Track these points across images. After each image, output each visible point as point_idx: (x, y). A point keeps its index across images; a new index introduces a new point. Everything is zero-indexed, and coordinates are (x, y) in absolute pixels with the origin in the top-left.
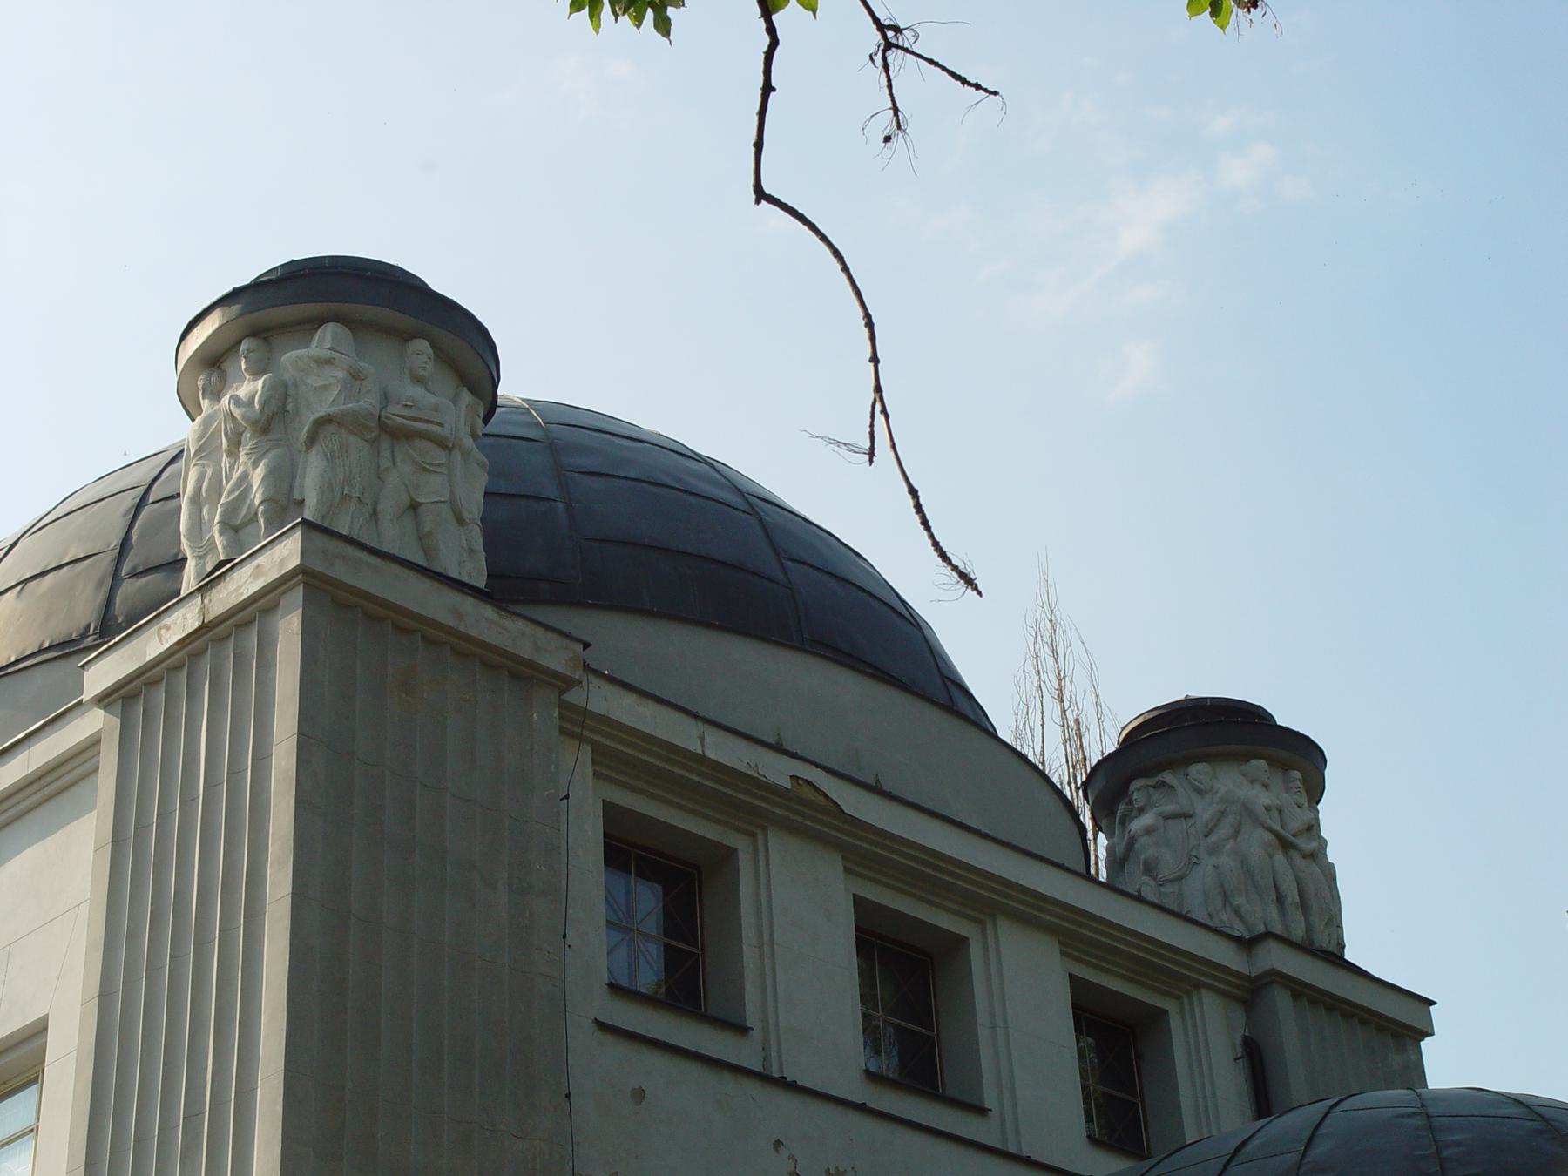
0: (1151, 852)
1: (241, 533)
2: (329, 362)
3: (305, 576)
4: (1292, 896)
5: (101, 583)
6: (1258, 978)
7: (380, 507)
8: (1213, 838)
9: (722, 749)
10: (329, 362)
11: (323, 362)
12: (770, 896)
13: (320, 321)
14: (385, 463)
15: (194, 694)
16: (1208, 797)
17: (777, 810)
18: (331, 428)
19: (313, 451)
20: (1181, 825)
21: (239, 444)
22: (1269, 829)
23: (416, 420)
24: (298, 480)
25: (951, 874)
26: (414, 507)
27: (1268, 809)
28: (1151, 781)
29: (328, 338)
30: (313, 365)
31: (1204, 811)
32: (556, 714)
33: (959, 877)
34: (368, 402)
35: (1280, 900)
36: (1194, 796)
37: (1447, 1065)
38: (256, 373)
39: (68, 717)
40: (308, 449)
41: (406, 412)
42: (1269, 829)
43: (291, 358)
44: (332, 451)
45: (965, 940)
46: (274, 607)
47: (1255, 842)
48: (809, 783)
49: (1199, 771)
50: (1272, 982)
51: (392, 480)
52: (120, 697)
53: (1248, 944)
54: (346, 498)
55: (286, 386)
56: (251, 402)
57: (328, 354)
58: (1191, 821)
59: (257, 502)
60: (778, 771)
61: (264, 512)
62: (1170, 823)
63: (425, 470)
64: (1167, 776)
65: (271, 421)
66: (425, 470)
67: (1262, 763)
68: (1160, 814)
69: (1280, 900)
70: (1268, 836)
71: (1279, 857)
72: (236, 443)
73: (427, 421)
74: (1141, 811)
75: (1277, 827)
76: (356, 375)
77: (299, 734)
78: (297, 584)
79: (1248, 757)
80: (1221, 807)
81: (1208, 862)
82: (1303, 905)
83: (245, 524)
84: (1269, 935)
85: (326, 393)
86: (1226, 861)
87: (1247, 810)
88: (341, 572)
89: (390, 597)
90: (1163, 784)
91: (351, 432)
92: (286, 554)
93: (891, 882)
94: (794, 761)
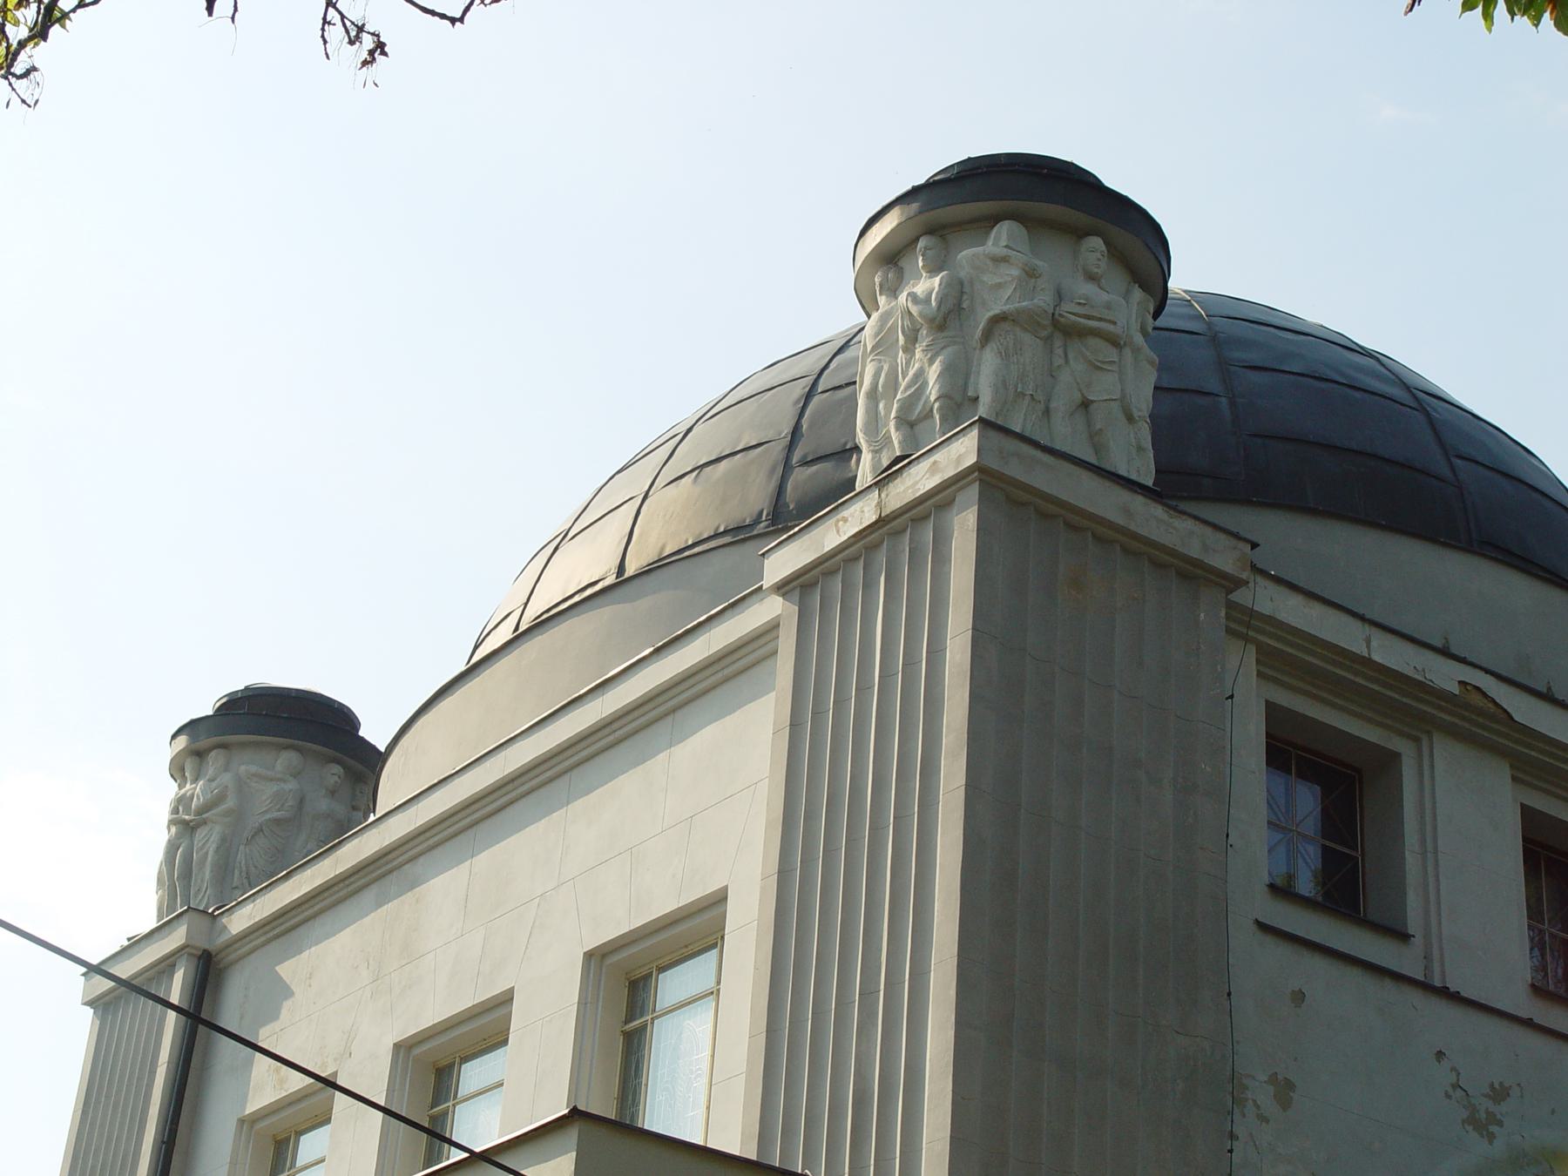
1: (918, 428)
2: (1005, 260)
3: (980, 472)
7: (1053, 405)
9: (1388, 653)
10: (1005, 260)
13: (995, 220)
15: (870, 586)
18: (1006, 326)
19: (988, 350)
21: (916, 340)
26: (1085, 404)
29: (1004, 236)
30: (989, 262)
34: (1043, 300)
38: (933, 270)
39: (747, 601)
43: (966, 255)
51: (1065, 377)
56: (928, 300)
57: (1005, 252)
59: (932, 398)
60: (1446, 675)
61: (940, 409)
65: (948, 318)
72: (912, 339)
73: (1100, 319)
76: (1031, 273)
85: (1000, 291)
88: (1015, 471)
89: (1064, 496)
91: (1026, 330)
92: (963, 451)
94: (1462, 666)
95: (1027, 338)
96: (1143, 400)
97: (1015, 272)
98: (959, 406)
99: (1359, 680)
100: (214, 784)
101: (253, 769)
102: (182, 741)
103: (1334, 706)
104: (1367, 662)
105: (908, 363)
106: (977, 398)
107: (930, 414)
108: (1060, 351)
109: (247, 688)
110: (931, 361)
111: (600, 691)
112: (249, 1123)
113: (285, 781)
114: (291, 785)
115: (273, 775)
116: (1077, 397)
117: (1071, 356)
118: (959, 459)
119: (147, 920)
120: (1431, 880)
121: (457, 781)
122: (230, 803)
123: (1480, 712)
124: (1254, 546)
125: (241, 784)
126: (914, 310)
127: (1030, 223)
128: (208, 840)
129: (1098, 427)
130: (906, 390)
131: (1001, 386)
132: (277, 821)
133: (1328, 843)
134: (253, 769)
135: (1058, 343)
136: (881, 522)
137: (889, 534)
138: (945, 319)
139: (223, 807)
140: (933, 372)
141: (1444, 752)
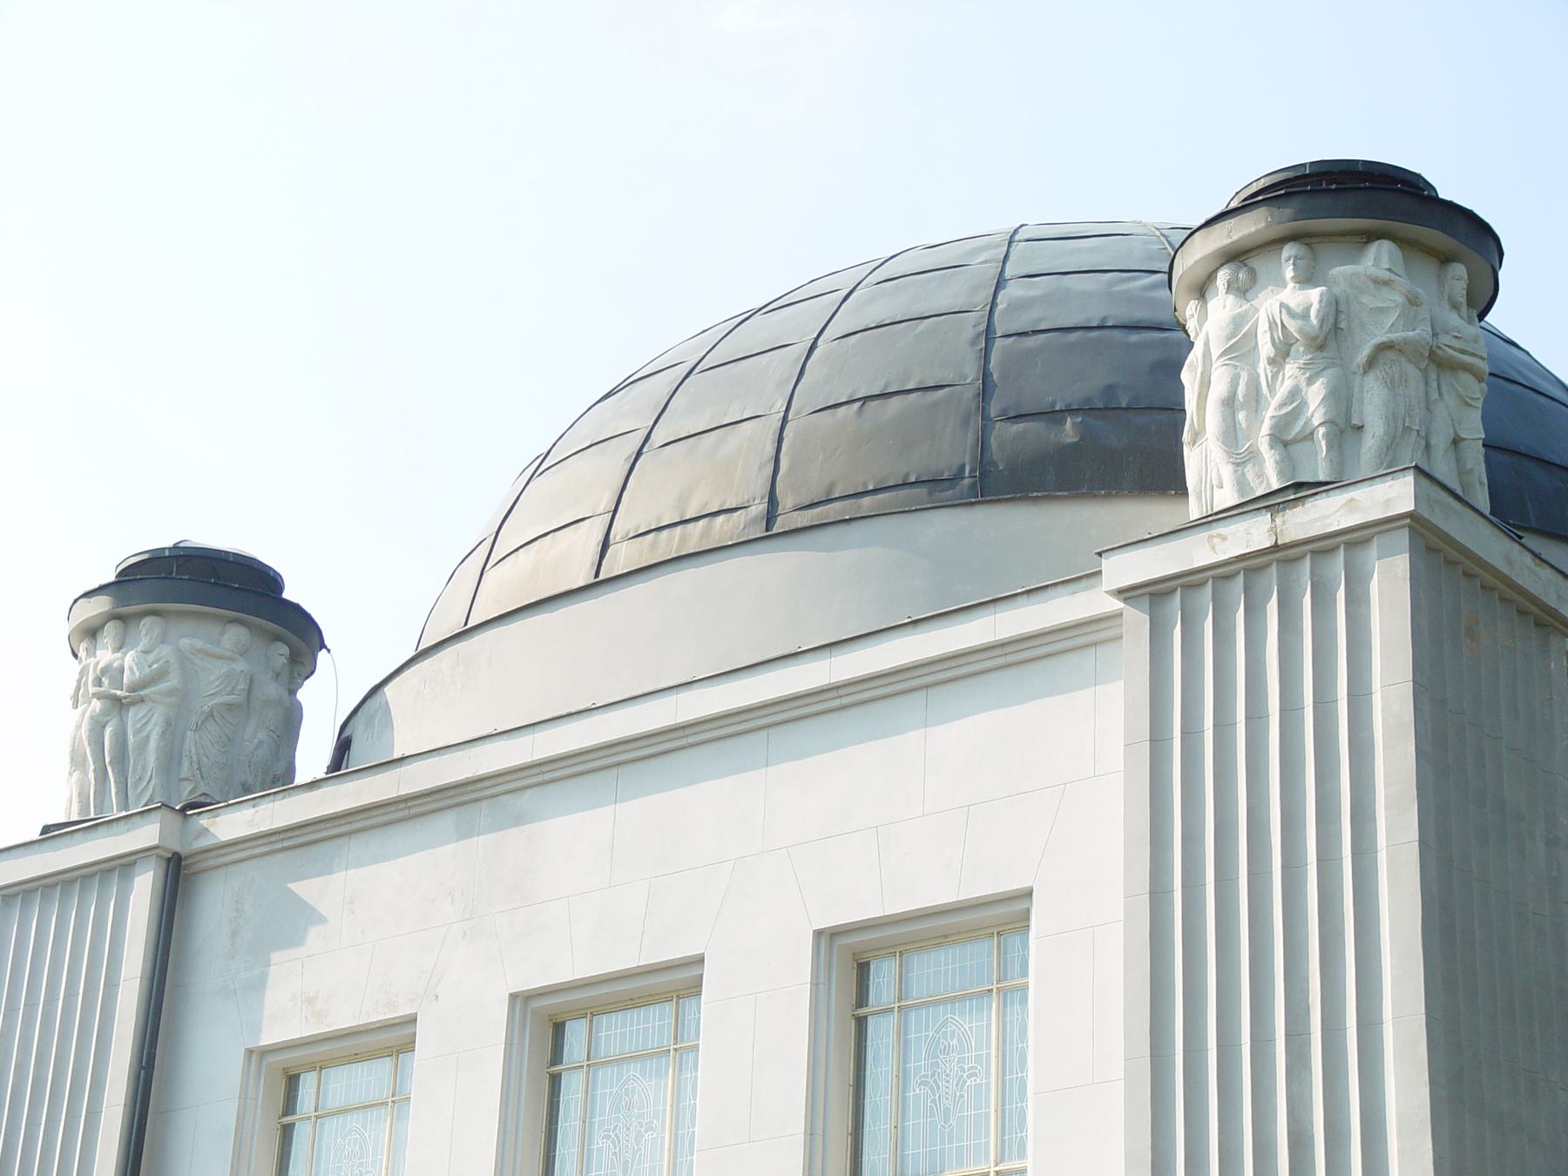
1: (1294, 449)
3: (1415, 523)
5: (966, 422)
13: (1370, 237)
14: (1435, 395)
18: (1390, 355)
19: (1371, 375)
23: (1462, 352)
24: (1355, 403)
29: (1385, 257)
34: (1421, 332)
37: (286, 595)
38: (1307, 279)
39: (1051, 592)
40: (1365, 372)
43: (1341, 271)
44: (1392, 380)
46: (1366, 541)
51: (1441, 412)
52: (1152, 594)
54: (1407, 429)
56: (1305, 315)
57: (1387, 275)
59: (1316, 422)
61: (1326, 435)
63: (1467, 404)
65: (1328, 339)
66: (1467, 404)
72: (1283, 352)
73: (1473, 355)
76: (1413, 301)
83: (1295, 441)
85: (1383, 319)
88: (1437, 519)
91: (1410, 361)
92: (1397, 495)
96: (1474, 431)
97: (1400, 299)
98: (1342, 432)
100: (151, 657)
101: (199, 644)
102: (102, 605)
105: (1275, 376)
106: (1360, 428)
107: (1310, 436)
108: (1434, 384)
109: (175, 547)
110: (1310, 381)
111: (826, 652)
112: (258, 1055)
113: (233, 660)
114: (241, 665)
115: (216, 650)
118: (1388, 503)
119: (59, 800)
121: (596, 718)
122: (173, 681)
125: (183, 659)
126: (1293, 326)
128: (147, 725)
130: (1282, 405)
132: (230, 707)
134: (199, 644)
136: (1276, 548)
139: (163, 686)
140: (1315, 395)
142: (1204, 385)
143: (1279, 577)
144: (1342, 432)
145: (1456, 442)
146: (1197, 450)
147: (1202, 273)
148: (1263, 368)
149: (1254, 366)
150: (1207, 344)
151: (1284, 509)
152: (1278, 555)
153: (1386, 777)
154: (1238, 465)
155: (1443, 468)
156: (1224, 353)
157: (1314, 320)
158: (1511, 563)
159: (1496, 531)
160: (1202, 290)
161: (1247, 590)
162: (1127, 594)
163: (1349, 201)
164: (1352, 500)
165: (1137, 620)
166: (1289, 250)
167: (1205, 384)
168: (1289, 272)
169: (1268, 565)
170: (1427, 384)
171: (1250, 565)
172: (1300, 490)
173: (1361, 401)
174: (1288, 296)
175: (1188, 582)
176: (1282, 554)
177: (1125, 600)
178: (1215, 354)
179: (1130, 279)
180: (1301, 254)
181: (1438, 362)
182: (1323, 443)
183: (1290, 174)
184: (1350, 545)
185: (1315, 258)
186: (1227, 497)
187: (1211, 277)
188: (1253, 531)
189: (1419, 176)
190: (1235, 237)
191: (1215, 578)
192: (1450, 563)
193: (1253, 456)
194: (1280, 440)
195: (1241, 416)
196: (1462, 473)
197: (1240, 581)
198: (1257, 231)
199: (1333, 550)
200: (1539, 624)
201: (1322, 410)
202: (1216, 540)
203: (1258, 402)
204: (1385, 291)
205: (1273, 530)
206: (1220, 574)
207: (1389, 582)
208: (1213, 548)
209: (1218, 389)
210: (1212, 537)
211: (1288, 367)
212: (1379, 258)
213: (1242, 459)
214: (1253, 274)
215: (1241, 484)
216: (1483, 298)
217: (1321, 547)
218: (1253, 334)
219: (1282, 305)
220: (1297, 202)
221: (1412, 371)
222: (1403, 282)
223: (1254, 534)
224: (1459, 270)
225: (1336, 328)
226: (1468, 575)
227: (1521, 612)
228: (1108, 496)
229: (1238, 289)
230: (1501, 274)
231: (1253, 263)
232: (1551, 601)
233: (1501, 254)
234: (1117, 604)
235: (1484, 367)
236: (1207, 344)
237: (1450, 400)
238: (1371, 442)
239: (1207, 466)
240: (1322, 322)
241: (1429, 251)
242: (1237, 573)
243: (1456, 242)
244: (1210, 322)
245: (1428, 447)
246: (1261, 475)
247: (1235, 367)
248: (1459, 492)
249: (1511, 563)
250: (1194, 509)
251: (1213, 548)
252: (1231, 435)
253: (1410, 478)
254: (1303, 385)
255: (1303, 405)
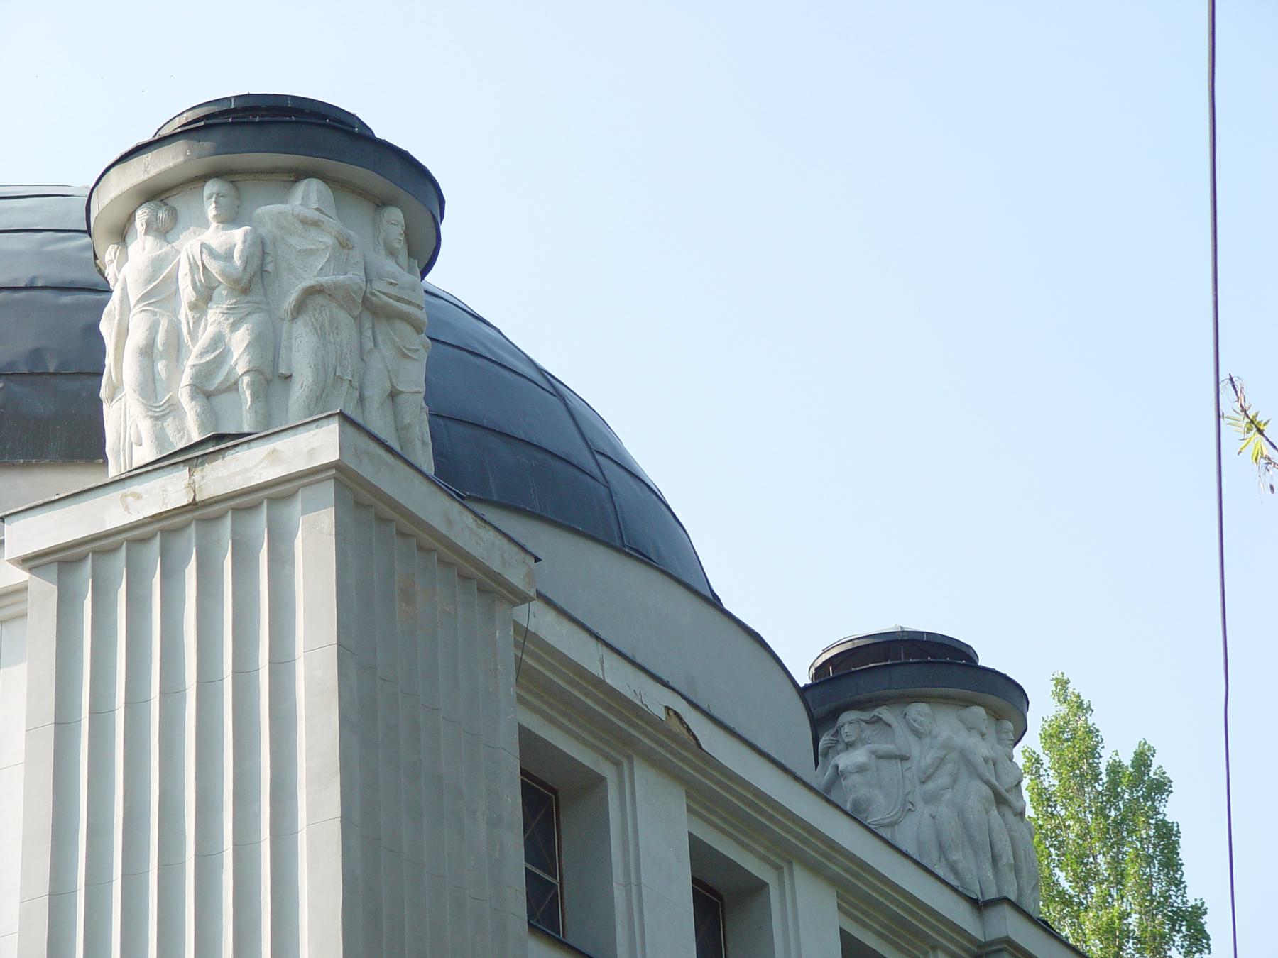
0: (862, 792)
1: (216, 400)
2: (315, 224)
3: (339, 473)
4: (1007, 858)
6: (988, 944)
7: (367, 393)
8: (930, 786)
9: (619, 677)
10: (315, 224)
11: (308, 223)
12: (636, 831)
13: (299, 175)
14: (369, 345)
15: (171, 577)
16: (928, 741)
17: (646, 741)
18: (320, 300)
20: (895, 767)
21: (209, 299)
22: (987, 783)
23: (399, 299)
24: (283, 353)
25: (770, 818)
26: (393, 395)
27: (986, 760)
28: (866, 716)
30: (300, 226)
31: (922, 755)
32: (512, 633)
33: (777, 822)
34: (354, 276)
35: (995, 860)
36: (912, 739)
38: (230, 219)
40: (294, 319)
41: (390, 290)
42: (987, 783)
43: (268, 211)
44: (322, 326)
45: (765, 885)
46: (291, 496)
47: (975, 794)
48: (676, 713)
49: (918, 711)
50: (1001, 950)
52: (59, 562)
53: (980, 906)
55: (263, 244)
58: (907, 764)
59: (240, 370)
60: (656, 700)
61: (251, 384)
62: (883, 763)
64: (884, 713)
65: (254, 281)
67: (980, 711)
68: (873, 752)
69: (995, 860)
70: (986, 790)
71: (994, 812)
72: (205, 296)
73: (410, 303)
74: (850, 745)
75: (994, 781)
76: (344, 244)
77: (339, 644)
78: (328, 479)
79: (967, 703)
80: (941, 754)
81: (924, 811)
82: (1017, 870)
84: (1006, 900)
86: (944, 811)
87: (966, 759)
88: (366, 471)
89: (403, 500)
90: (878, 720)
91: (341, 307)
92: (321, 444)
93: (714, 819)
94: (666, 690)
95: (343, 316)
96: (413, 379)
97: (329, 240)
98: (269, 382)
99: (589, 702)
103: (568, 731)
104: (599, 683)
105: (197, 322)
106: (288, 378)
107: (233, 387)
108: (369, 333)
110: (234, 327)
116: (388, 387)
117: (380, 339)
118: (311, 452)
120: (636, 915)
123: (683, 744)
124: (537, 560)
126: (214, 267)
127: (336, 184)
129: (407, 421)
130: (204, 352)
131: (321, 367)
133: (530, 867)
135: (367, 324)
136: (194, 505)
137: (197, 520)
138: (250, 281)
140: (239, 341)
141: (645, 780)
142: (124, 330)
143: (198, 538)
144: (269, 382)
145: (393, 395)
146: (115, 405)
147: (119, 214)
148: (184, 314)
149: (175, 312)
150: (124, 289)
151: (203, 464)
152: (196, 514)
153: (308, 750)
154: (157, 418)
155: (378, 422)
156: (143, 298)
157: (237, 261)
158: (450, 523)
159: (434, 488)
160: (122, 234)
161: (164, 553)
162: (32, 562)
163: (273, 139)
164: (274, 451)
165: (44, 591)
166: (211, 187)
167: (123, 333)
168: (211, 211)
169: (186, 526)
170: (361, 332)
171: (166, 526)
172: (221, 441)
173: (290, 348)
174: (212, 236)
175: (99, 546)
176: (200, 512)
177: (31, 570)
178: (133, 301)
179: (65, 239)
180: (223, 191)
181: (372, 310)
182: (248, 393)
183: (214, 109)
184: (274, 500)
185: (237, 188)
186: (146, 454)
187: (131, 218)
188: (170, 488)
189: (353, 116)
190: (153, 172)
191: (129, 541)
192: (382, 520)
193: (173, 408)
194: (203, 391)
195: (161, 366)
196: (400, 428)
197: (157, 543)
198: (175, 166)
199: (255, 507)
200: (482, 590)
201: (246, 358)
202: (130, 499)
203: (179, 351)
204: (314, 232)
205: (191, 486)
206: (133, 537)
207: (314, 536)
208: (127, 508)
209: (136, 338)
210: (125, 496)
211: (210, 312)
212: (308, 197)
213: (161, 412)
214: (173, 213)
215: (160, 438)
216: (425, 253)
217: (243, 503)
218: (173, 278)
219: (203, 245)
220: (218, 134)
221: (343, 317)
222: (333, 224)
223: (170, 491)
224: (395, 214)
225: (262, 271)
226: (402, 534)
227: (462, 577)
228: (27, 465)
229: (158, 230)
230: (444, 227)
231: (173, 201)
232: (496, 566)
233: (442, 202)
234: (21, 576)
235: (422, 315)
236: (124, 289)
237: (387, 351)
238: (299, 392)
239: (127, 426)
240: (246, 264)
241: (363, 193)
242: (153, 536)
243: (388, 184)
244: (128, 267)
245: (361, 399)
246: (181, 429)
247: (155, 313)
248: (398, 448)
249: (450, 523)
250: (113, 471)
251: (127, 508)
252: (149, 387)
253: (334, 427)
254: (226, 330)
255: (226, 353)
